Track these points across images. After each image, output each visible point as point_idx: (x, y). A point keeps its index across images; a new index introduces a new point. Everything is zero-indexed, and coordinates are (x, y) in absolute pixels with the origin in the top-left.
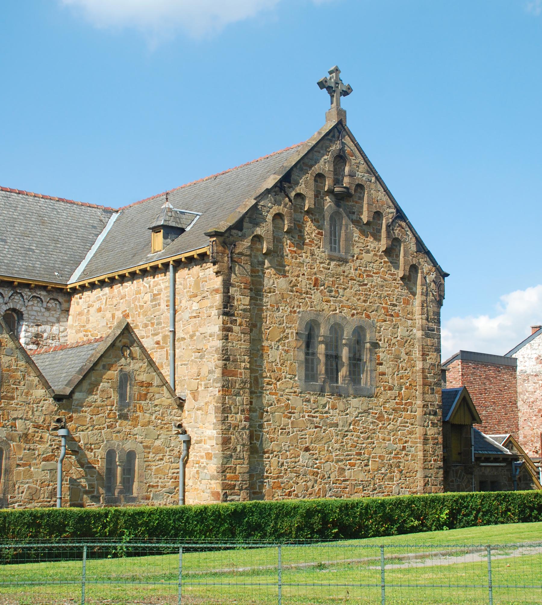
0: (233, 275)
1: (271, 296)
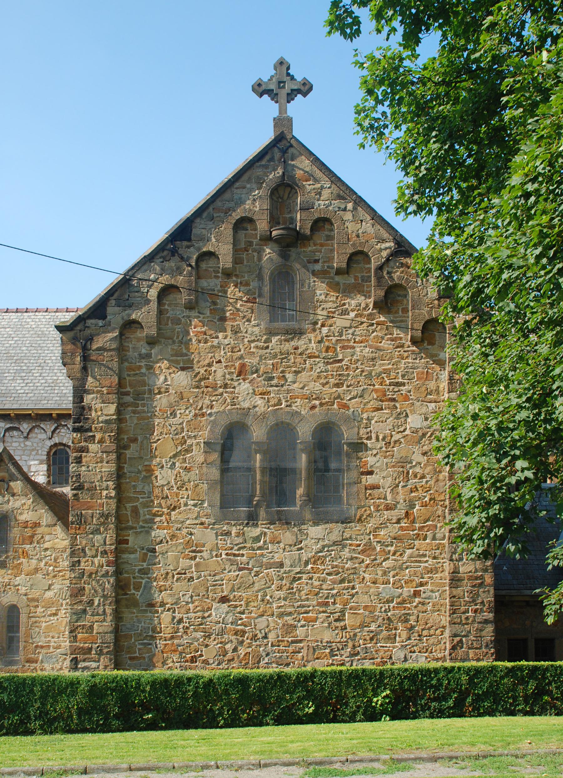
0: (90, 379)
1: (160, 398)
